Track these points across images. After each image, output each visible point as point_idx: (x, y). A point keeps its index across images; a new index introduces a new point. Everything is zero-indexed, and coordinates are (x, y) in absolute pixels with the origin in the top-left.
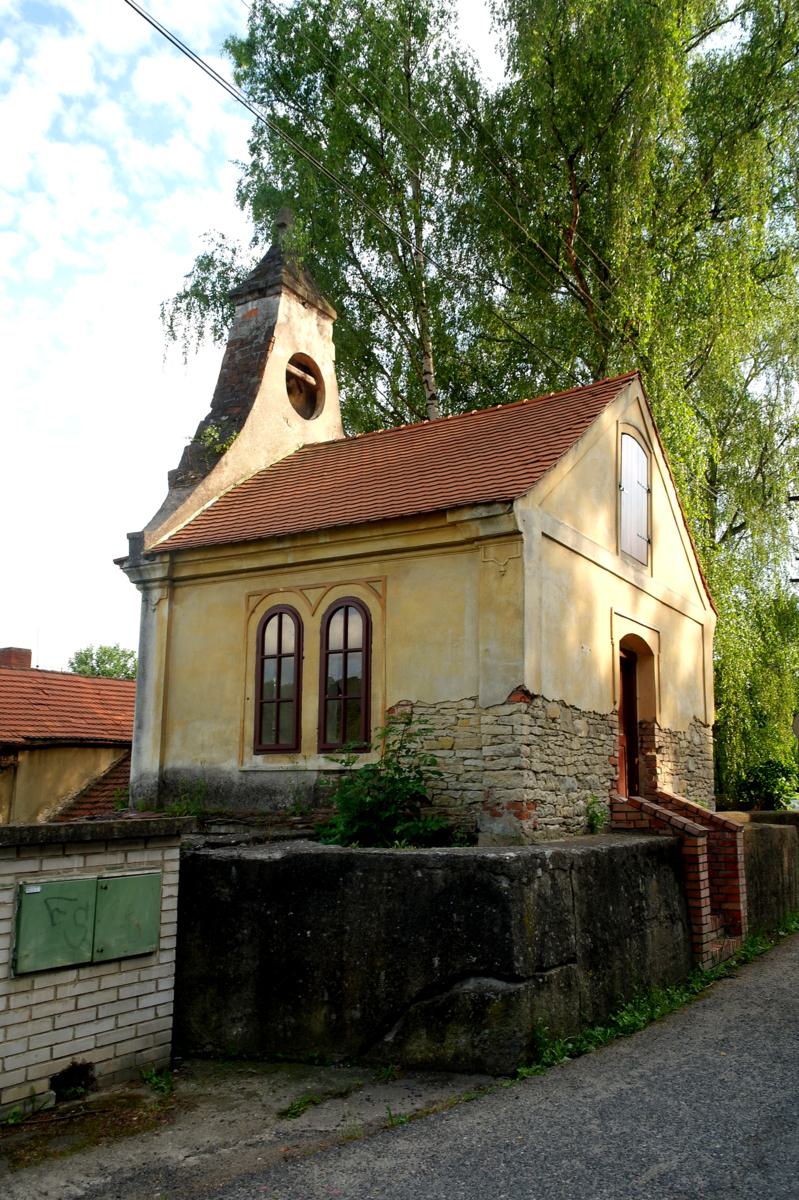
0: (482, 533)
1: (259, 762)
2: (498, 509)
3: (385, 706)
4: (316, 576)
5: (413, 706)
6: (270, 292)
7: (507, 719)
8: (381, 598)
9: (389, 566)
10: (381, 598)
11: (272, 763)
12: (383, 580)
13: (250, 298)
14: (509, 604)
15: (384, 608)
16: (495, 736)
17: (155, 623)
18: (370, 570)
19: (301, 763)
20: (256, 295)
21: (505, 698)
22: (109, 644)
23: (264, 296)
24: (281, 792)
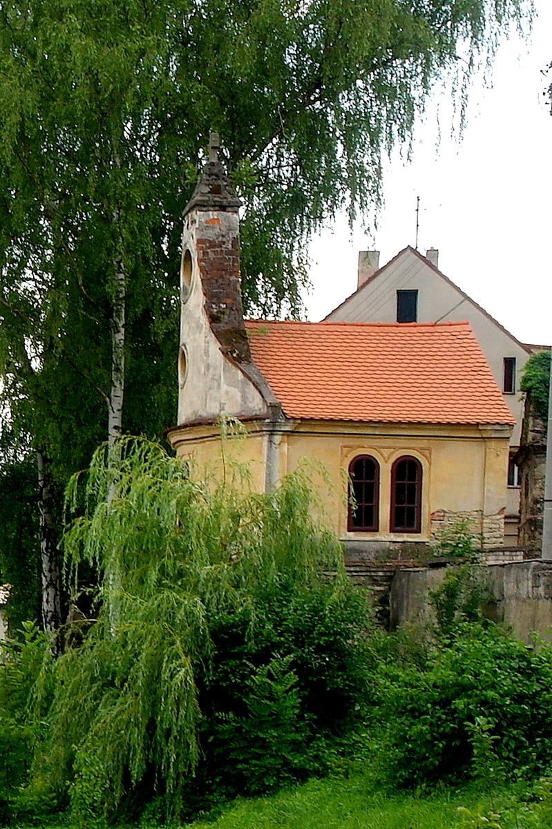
0: (493, 436)
1: (351, 535)
2: (507, 427)
3: (429, 512)
4: (389, 442)
5: (444, 512)
6: (229, 209)
7: (496, 521)
8: (429, 459)
9: (433, 442)
10: (429, 459)
11: (360, 536)
12: (429, 450)
13: (212, 209)
14: (500, 469)
15: (430, 464)
16: (490, 528)
17: (277, 455)
18: (423, 443)
19: (378, 537)
20: (217, 208)
21: (497, 512)
22: (546, 528)
23: (224, 210)
24: (366, 552)
